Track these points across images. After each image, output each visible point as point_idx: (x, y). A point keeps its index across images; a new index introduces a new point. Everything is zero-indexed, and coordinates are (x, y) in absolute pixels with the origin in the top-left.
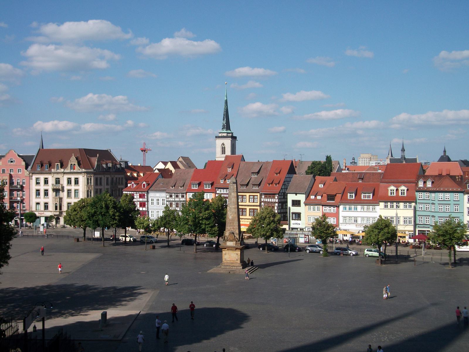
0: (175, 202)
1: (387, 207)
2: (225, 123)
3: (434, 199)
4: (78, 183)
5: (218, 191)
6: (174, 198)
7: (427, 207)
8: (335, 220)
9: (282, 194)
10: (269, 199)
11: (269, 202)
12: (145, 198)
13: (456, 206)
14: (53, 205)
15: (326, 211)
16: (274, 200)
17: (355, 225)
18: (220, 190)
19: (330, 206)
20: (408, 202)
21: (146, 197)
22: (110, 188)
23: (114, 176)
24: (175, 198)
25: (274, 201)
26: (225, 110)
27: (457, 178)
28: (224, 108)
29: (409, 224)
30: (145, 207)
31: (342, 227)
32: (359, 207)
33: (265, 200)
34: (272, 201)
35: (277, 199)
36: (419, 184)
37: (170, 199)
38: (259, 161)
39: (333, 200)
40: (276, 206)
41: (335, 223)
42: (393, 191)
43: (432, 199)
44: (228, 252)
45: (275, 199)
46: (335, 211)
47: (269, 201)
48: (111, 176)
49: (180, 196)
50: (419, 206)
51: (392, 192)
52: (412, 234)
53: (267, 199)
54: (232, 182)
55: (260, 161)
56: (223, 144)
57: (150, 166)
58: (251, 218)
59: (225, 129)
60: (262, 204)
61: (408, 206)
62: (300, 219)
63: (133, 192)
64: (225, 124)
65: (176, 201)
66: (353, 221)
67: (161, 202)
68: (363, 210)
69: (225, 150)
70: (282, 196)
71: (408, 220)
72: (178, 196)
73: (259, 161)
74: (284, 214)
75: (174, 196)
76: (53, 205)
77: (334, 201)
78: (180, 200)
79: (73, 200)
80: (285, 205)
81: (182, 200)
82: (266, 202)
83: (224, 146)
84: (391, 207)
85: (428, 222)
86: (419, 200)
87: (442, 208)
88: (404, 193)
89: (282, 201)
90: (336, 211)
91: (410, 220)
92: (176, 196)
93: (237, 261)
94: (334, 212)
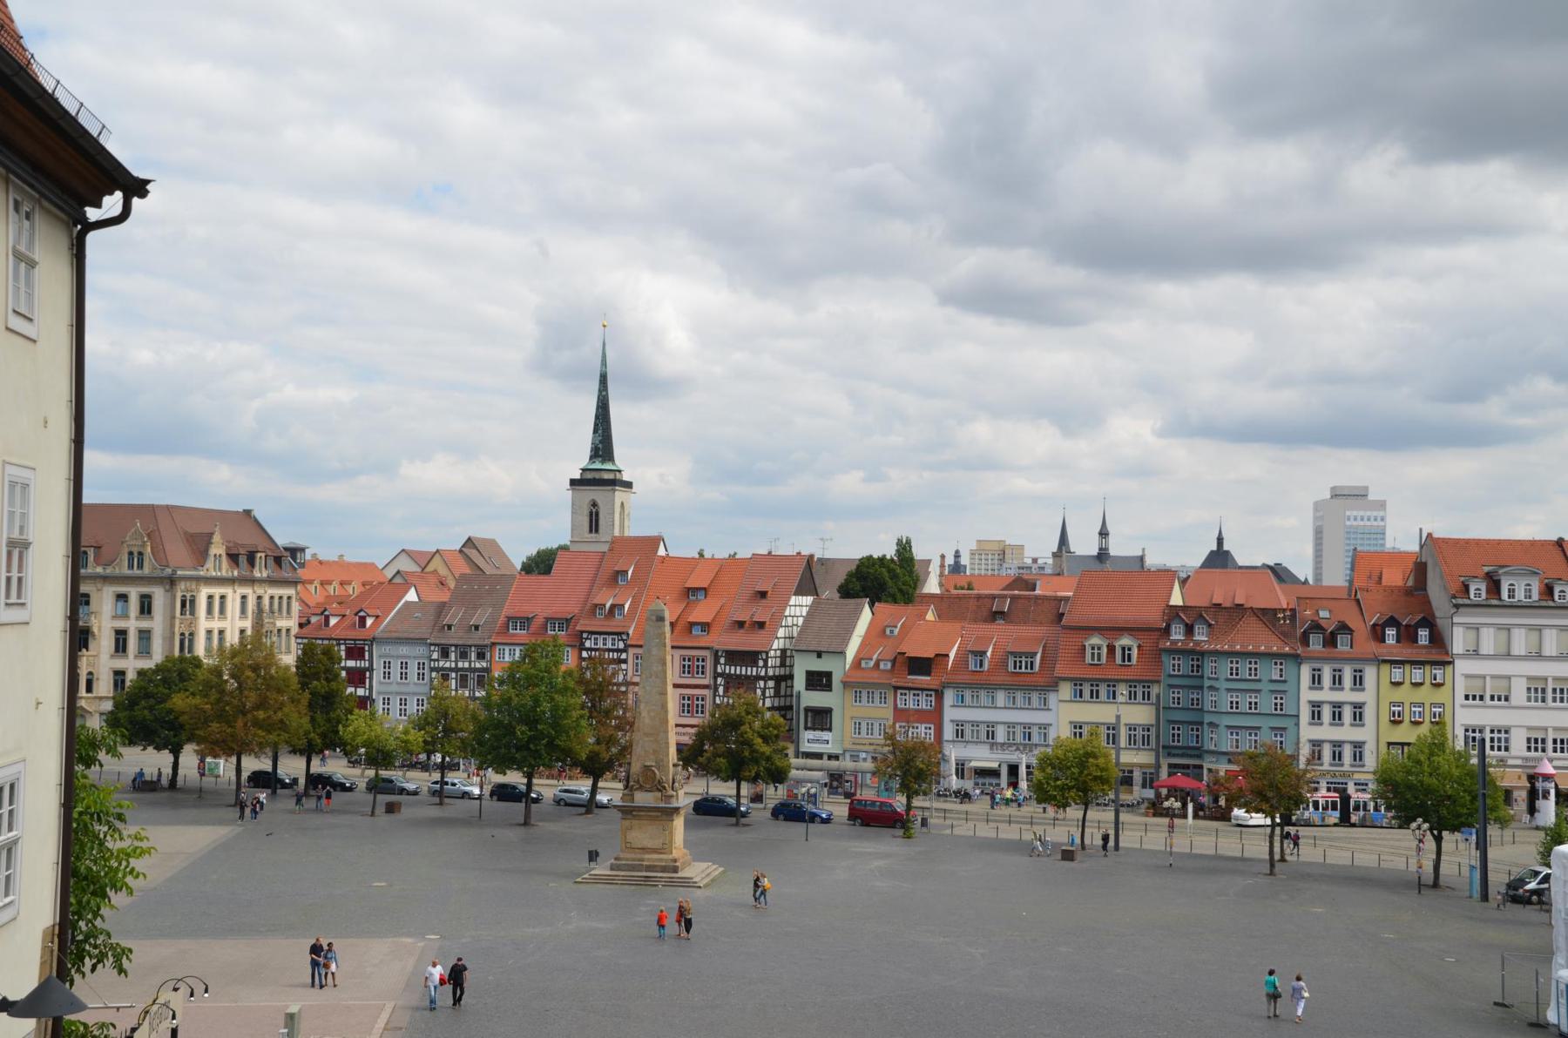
0: (456, 672)
1: (1097, 697)
3: (1214, 676)
4: (149, 612)
6: (453, 659)
7: (1176, 695)
8: (932, 731)
9: (778, 653)
10: (738, 668)
11: (741, 675)
12: (365, 660)
13: (1279, 696)
14: (69, 403)
15: (918, 705)
16: (755, 669)
17: (988, 747)
18: (593, 637)
20: (1140, 681)
21: (367, 657)
22: (253, 627)
23: (266, 592)
24: (456, 662)
25: (754, 673)
27: (1281, 615)
29: (1143, 744)
30: (365, 687)
31: (953, 753)
32: (1001, 698)
33: (727, 671)
34: (749, 673)
35: (762, 668)
36: (1197, 631)
37: (441, 664)
38: (701, 554)
40: (760, 688)
42: (1099, 649)
43: (1172, 673)
44: (637, 822)
45: (758, 667)
47: (738, 672)
49: (473, 654)
50: (1191, 696)
51: (1096, 651)
52: (1151, 774)
53: (749, 669)
54: (654, 618)
55: (707, 555)
56: (594, 504)
57: (373, 564)
58: (474, 551)
59: (600, 459)
60: (719, 680)
62: (809, 725)
63: (320, 639)
65: (462, 669)
66: (983, 736)
67: (413, 670)
68: (1014, 704)
69: (597, 521)
70: (778, 660)
71: (1139, 733)
72: (466, 653)
73: (701, 554)
75: (453, 654)
76: (68, 561)
78: (473, 666)
79: (132, 665)
80: (787, 687)
81: (478, 665)
82: (729, 675)
83: (594, 510)
84: (1092, 697)
85: (1179, 741)
86: (1209, 678)
88: (1099, 654)
89: (777, 674)
90: (933, 704)
92: (461, 653)
93: (662, 851)
94: (929, 707)
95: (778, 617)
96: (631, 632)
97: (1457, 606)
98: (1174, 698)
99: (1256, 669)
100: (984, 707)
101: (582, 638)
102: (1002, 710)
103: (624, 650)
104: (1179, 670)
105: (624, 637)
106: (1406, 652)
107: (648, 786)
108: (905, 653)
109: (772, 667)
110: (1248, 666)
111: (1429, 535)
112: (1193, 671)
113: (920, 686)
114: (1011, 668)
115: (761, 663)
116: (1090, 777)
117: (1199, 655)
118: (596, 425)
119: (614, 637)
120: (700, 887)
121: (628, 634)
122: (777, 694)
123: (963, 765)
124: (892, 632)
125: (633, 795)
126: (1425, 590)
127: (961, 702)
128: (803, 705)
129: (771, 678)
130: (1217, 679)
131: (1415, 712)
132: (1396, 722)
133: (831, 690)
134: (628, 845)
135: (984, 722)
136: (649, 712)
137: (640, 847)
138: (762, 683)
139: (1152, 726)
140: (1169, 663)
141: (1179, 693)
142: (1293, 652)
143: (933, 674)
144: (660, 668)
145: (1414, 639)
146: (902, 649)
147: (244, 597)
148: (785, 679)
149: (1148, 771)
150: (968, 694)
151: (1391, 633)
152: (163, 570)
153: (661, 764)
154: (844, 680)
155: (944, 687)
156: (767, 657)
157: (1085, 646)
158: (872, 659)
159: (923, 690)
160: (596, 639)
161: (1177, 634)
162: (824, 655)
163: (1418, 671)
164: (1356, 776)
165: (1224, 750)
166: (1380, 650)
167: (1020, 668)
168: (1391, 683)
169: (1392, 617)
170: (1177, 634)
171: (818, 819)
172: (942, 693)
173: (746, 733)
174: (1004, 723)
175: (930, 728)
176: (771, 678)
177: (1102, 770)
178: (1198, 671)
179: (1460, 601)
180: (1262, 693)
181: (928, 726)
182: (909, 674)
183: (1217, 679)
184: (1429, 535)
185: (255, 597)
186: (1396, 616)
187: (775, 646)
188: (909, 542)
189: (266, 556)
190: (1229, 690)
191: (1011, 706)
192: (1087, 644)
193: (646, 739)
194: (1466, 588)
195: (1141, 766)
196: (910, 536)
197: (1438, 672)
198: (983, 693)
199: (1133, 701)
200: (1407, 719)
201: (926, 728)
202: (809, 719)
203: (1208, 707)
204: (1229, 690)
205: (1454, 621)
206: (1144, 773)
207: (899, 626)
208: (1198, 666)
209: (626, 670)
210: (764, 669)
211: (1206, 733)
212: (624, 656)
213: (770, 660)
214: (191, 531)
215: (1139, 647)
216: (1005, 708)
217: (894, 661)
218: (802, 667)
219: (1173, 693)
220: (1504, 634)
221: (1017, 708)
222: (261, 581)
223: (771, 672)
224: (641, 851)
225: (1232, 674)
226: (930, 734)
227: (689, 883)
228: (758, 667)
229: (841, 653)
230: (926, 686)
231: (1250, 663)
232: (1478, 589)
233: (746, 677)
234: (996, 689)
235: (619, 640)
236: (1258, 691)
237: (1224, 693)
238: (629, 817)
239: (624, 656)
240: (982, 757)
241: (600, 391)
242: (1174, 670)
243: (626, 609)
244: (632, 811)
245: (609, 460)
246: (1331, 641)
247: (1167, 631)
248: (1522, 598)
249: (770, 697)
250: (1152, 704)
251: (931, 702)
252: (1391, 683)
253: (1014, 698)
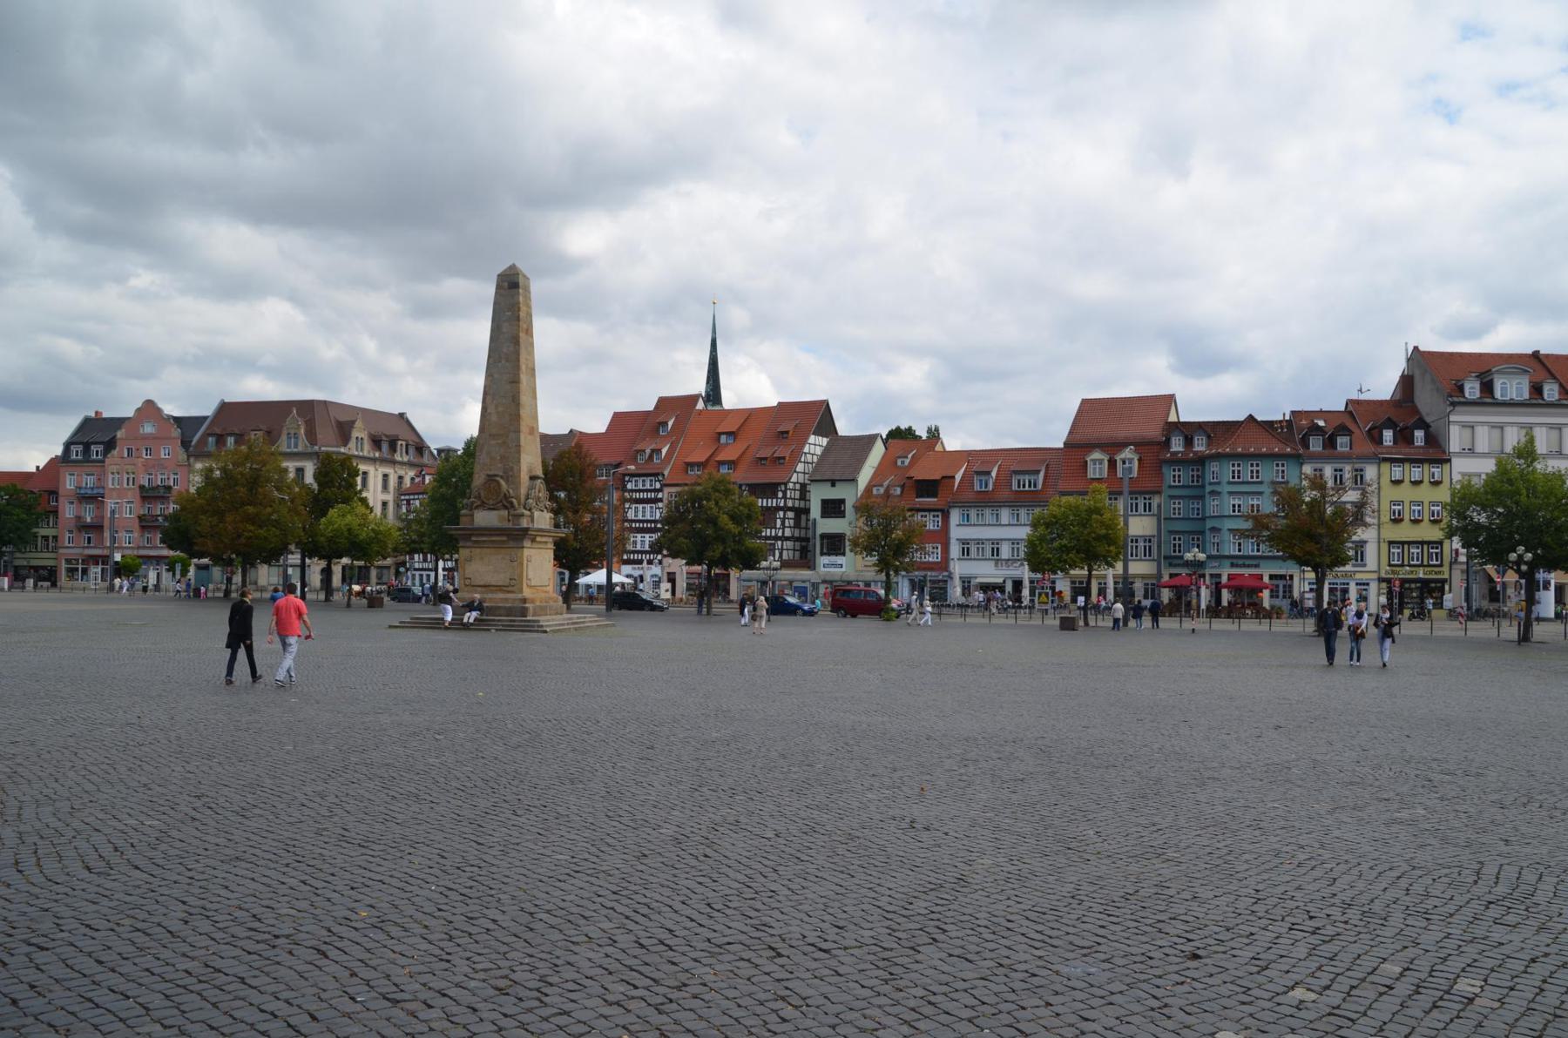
9: (798, 487)
17: (993, 563)
18: (634, 479)
31: (959, 568)
32: (1005, 515)
43: (1173, 484)
44: (478, 550)
48: (396, 472)
52: (1152, 584)
54: (506, 284)
61: (1141, 507)
62: (825, 551)
66: (988, 553)
86: (1211, 484)
87: (1179, 509)
91: (996, 546)
93: (510, 589)
95: (797, 455)
96: (666, 473)
97: (1453, 404)
98: (1174, 509)
99: (1258, 472)
100: (989, 525)
101: (624, 481)
102: (1008, 528)
103: (660, 490)
104: (1179, 481)
105: (660, 478)
106: (1403, 452)
107: (491, 502)
109: (791, 498)
110: (1250, 468)
111: (1416, 348)
112: (1193, 481)
113: (926, 507)
114: (1015, 487)
115: (780, 495)
116: (1093, 535)
117: (1201, 461)
118: (708, 377)
120: (545, 632)
121: (663, 475)
122: (797, 525)
123: (969, 582)
124: (903, 462)
125: (472, 515)
126: (1413, 402)
127: (966, 521)
129: (790, 509)
130: (1219, 483)
131: (1414, 511)
132: (1397, 521)
134: (468, 582)
135: (989, 540)
136: (497, 406)
137: (482, 583)
138: (781, 514)
139: (1154, 536)
140: (1170, 474)
141: (1179, 503)
142: (1294, 452)
144: (511, 349)
145: (1409, 440)
146: (913, 473)
148: (802, 512)
149: (1149, 582)
150: (973, 513)
151: (1388, 435)
155: (950, 507)
156: (786, 489)
157: (1086, 462)
158: (882, 486)
159: (930, 510)
160: (636, 481)
161: (1177, 445)
163: (1416, 469)
164: (1358, 576)
165: (1227, 554)
166: (1380, 450)
167: (1024, 486)
168: (1392, 481)
169: (1389, 419)
170: (1177, 445)
171: (800, 612)
172: (948, 512)
173: (711, 509)
174: (1009, 540)
176: (790, 509)
177: (1108, 527)
178: (1198, 481)
179: (1456, 399)
180: (1264, 496)
183: (1219, 483)
184: (1416, 348)
186: (1394, 419)
187: (794, 479)
188: (937, 429)
190: (1231, 493)
191: (1015, 522)
192: (1088, 459)
193: (493, 442)
194: (1461, 389)
195: (1143, 577)
196: (938, 424)
197: (1436, 471)
198: (987, 512)
200: (1407, 517)
202: (825, 546)
203: (1210, 511)
204: (1231, 493)
205: (1451, 419)
206: (1146, 584)
207: (910, 456)
208: (1198, 476)
211: (1208, 538)
212: (660, 495)
214: (341, 420)
215: (1140, 460)
216: (1009, 525)
217: (903, 487)
218: (817, 495)
219: (1174, 503)
220: (1497, 432)
221: (1021, 525)
223: (790, 504)
224: (483, 589)
225: (1233, 477)
227: (533, 626)
228: (777, 498)
230: (932, 507)
231: (1252, 465)
232: (1472, 389)
233: (768, 508)
234: (1000, 506)
236: (1260, 493)
237: (1226, 496)
238: (469, 544)
239: (660, 495)
240: (986, 572)
241: (711, 352)
242: (1174, 481)
243: (664, 454)
244: (471, 535)
246: (1330, 443)
247: (1167, 443)
248: (1514, 397)
250: (1154, 515)
252: (1392, 481)
253: (1018, 515)
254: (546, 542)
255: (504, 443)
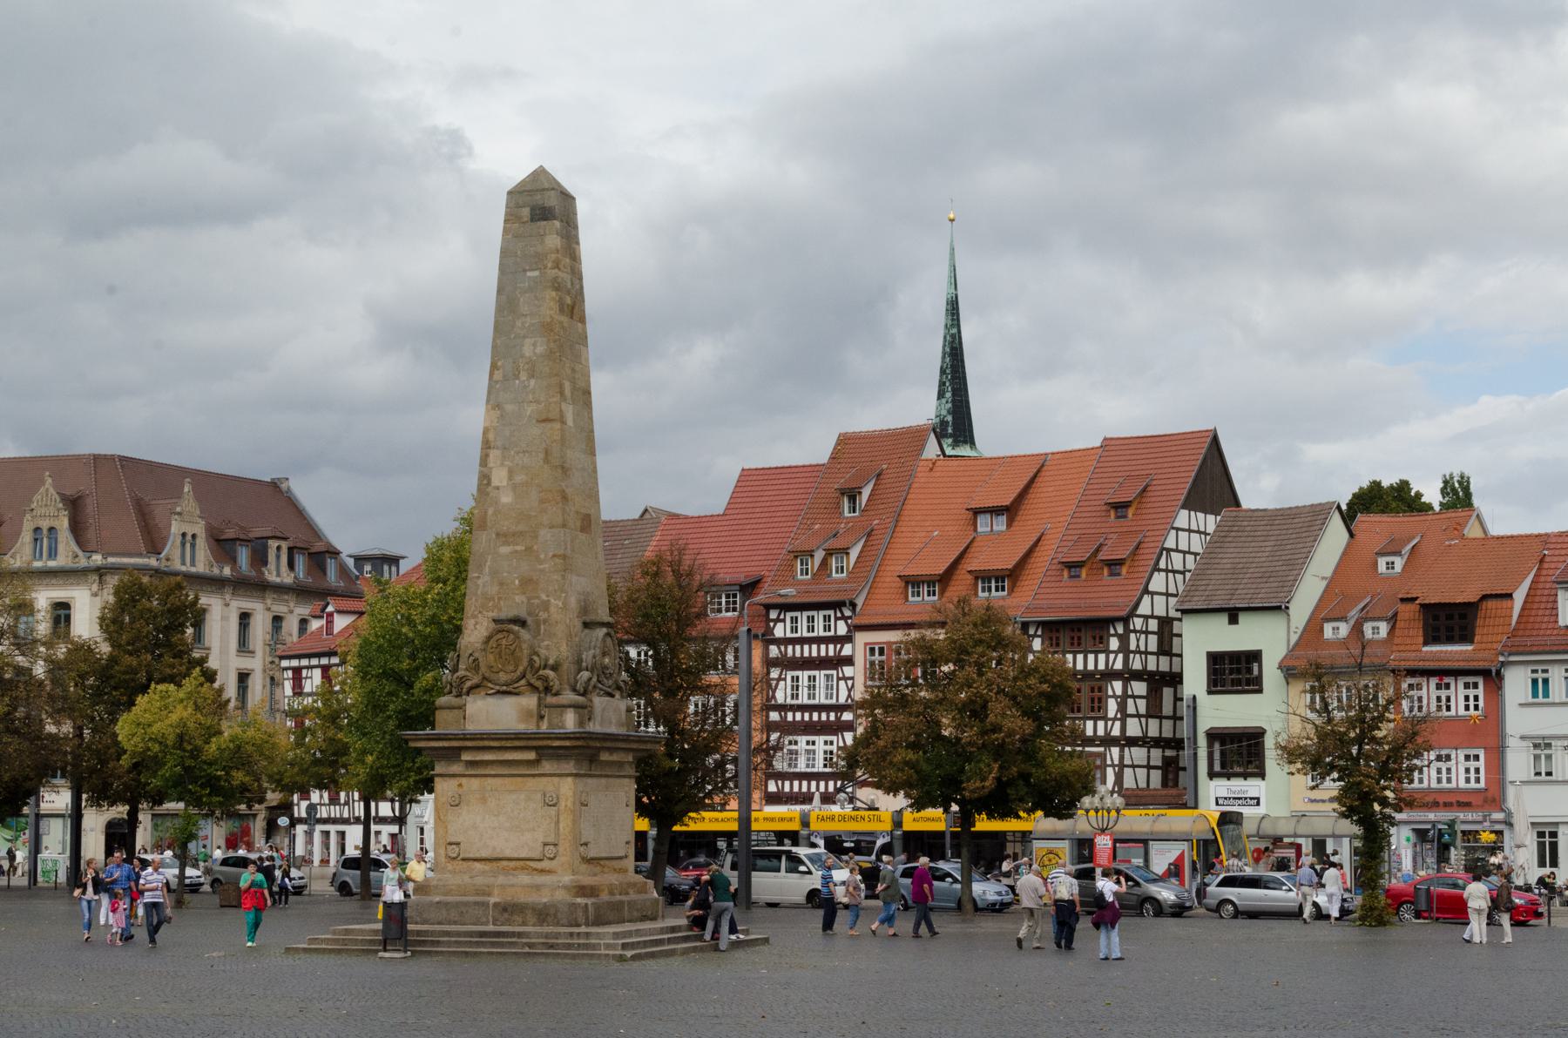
2: (949, 412)
5: (780, 626)
8: (1481, 764)
9: (1153, 625)
18: (789, 615)
19: (1443, 674)
23: (291, 612)
25: (1101, 666)
26: (948, 350)
28: (945, 337)
35: (1116, 653)
39: (1466, 637)
40: (1114, 696)
41: (1482, 785)
44: (475, 783)
46: (1476, 707)
54: (526, 212)
62: (1217, 768)
64: (949, 418)
74: (1169, 753)
77: (1471, 642)
90: (1481, 703)
93: (545, 864)
94: (1472, 711)
96: (860, 602)
101: (769, 620)
107: (503, 677)
108: (1416, 598)
109: (1138, 652)
115: (1114, 644)
119: (827, 612)
122: (1154, 712)
123: (1554, 835)
124: (1390, 565)
128: (1204, 725)
129: (1137, 676)
133: (1260, 691)
136: (511, 473)
137: (484, 854)
143: (1477, 638)
147: (245, 617)
152: (89, 558)
153: (543, 615)
154: (1291, 663)
156: (1127, 631)
162: (1242, 617)
175: (1477, 758)
176: (1137, 676)
181: (1472, 752)
182: (1426, 643)
185: (269, 616)
189: (290, 549)
193: (504, 550)
199: (1541, 699)
201: (1467, 758)
209: (852, 678)
210: (1120, 656)
212: (847, 650)
213: (1132, 636)
222: (280, 589)
226: (1477, 771)
229: (1278, 608)
235: (837, 619)
239: (847, 650)
245: (965, 442)
249: (1138, 716)
251: (1476, 698)
254: (620, 764)
255: (529, 549)
